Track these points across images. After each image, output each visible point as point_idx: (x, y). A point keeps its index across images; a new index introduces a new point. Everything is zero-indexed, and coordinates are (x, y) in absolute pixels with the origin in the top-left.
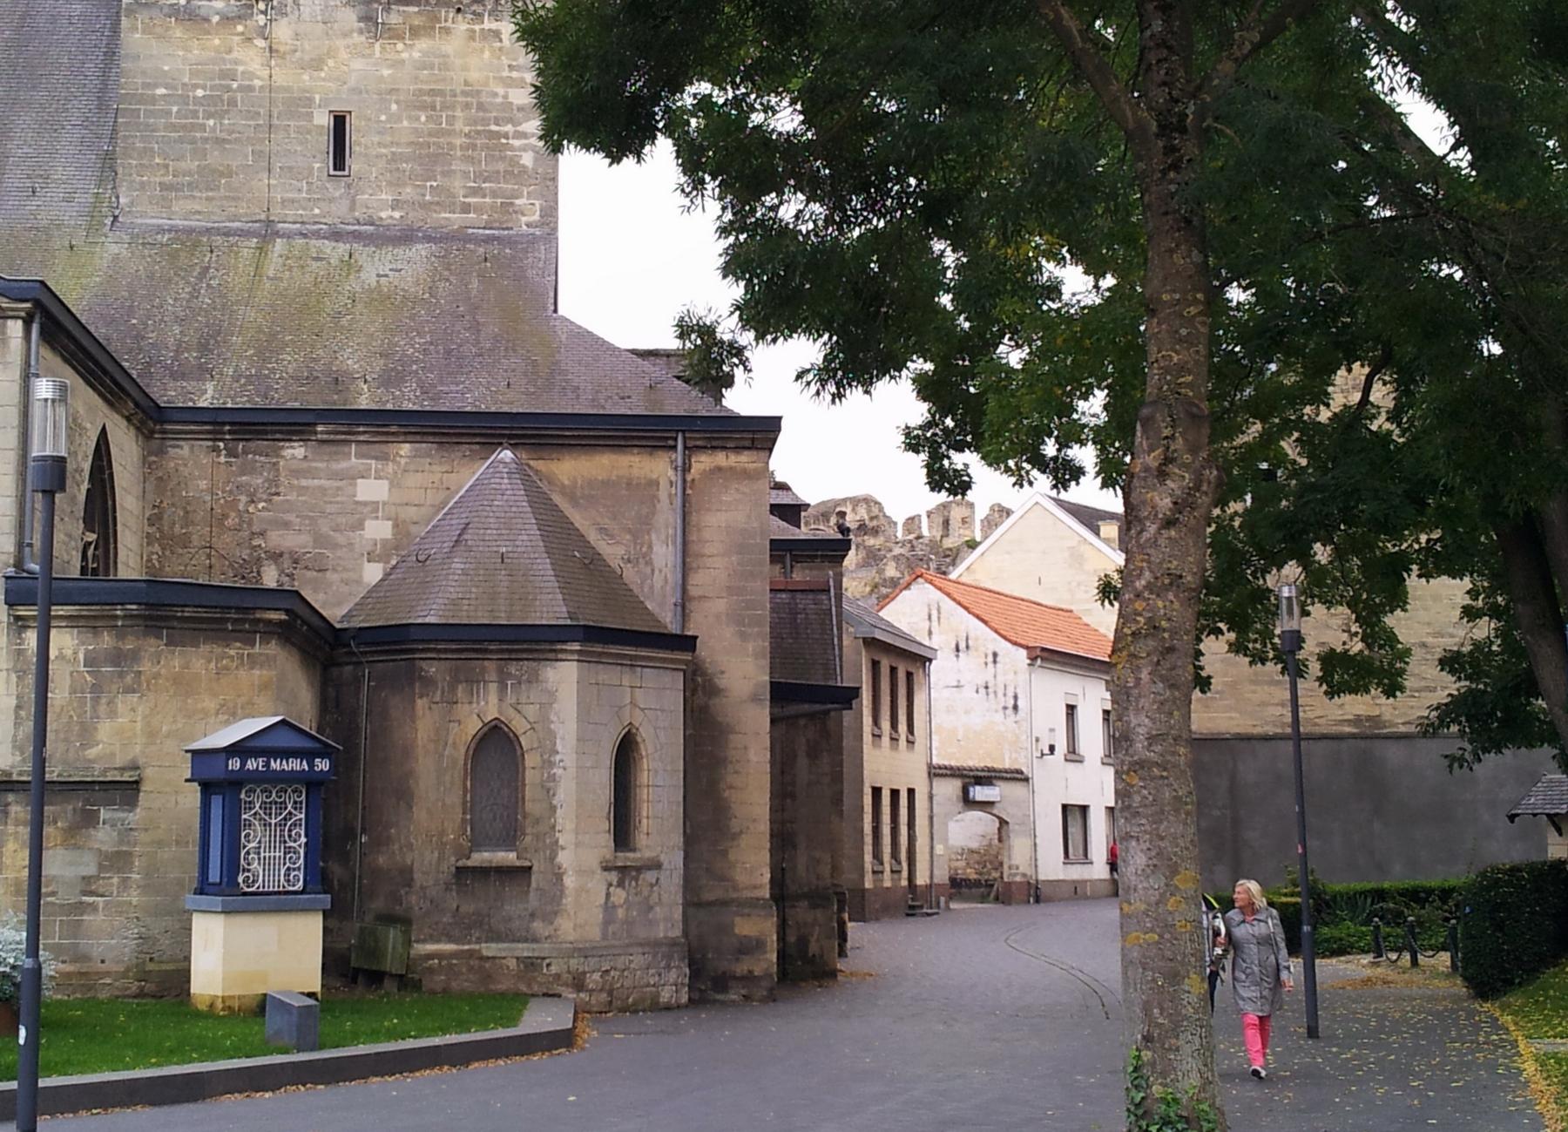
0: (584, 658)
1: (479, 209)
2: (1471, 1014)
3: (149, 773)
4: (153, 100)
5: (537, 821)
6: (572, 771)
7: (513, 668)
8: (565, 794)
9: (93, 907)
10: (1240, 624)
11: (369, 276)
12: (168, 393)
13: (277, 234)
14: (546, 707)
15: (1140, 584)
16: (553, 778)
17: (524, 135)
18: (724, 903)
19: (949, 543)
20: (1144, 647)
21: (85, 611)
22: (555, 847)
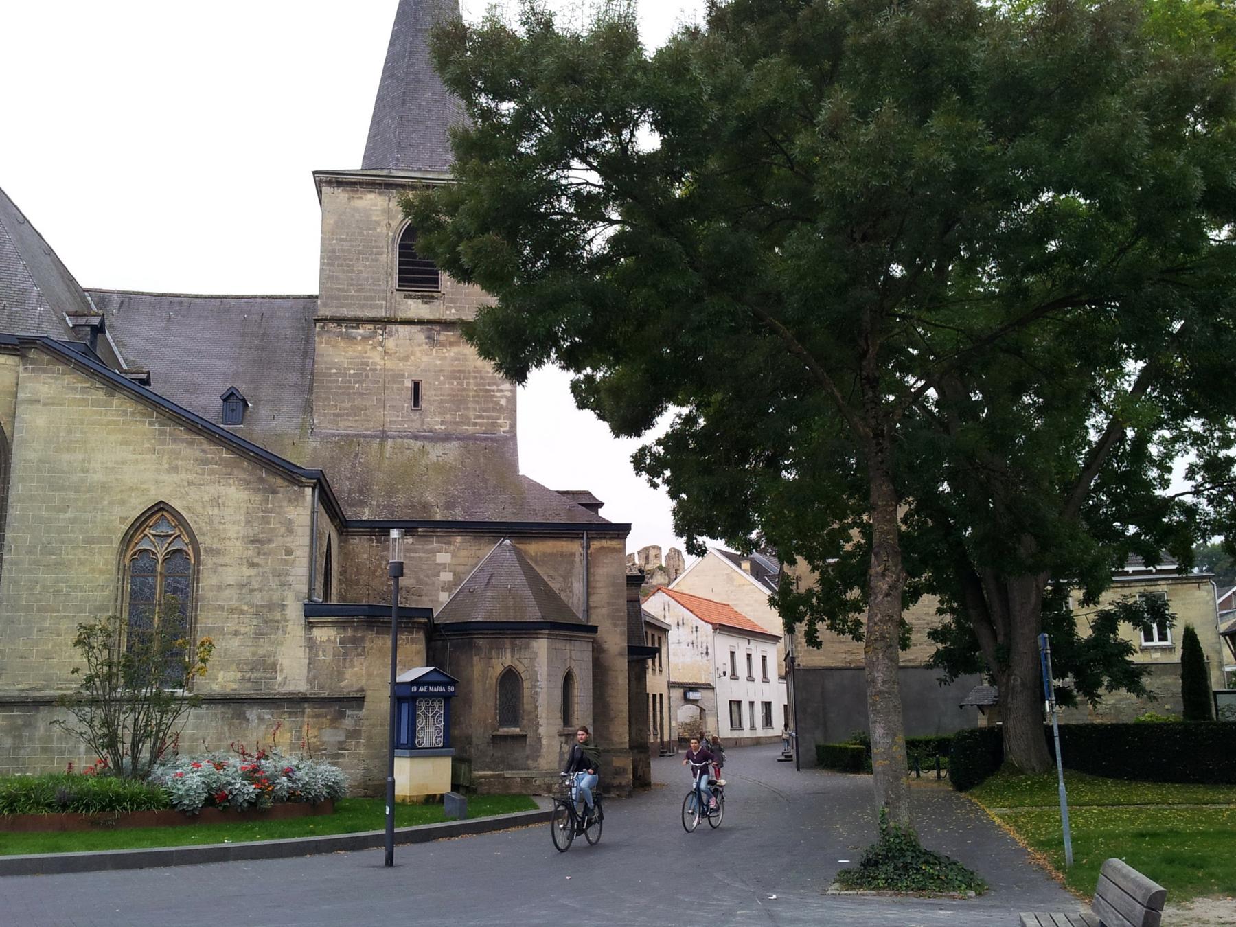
0: (550, 637)
1: (481, 425)
2: (958, 798)
3: (369, 693)
4: (331, 375)
5: (530, 713)
6: (545, 690)
7: (518, 642)
8: (542, 700)
9: (343, 755)
10: (833, 616)
11: (433, 457)
12: (349, 513)
13: (388, 437)
14: (533, 659)
15: (876, 619)
16: (536, 693)
17: (502, 391)
18: (608, 751)
19: (648, 567)
20: (880, 645)
21: (340, 619)
22: (537, 725)
